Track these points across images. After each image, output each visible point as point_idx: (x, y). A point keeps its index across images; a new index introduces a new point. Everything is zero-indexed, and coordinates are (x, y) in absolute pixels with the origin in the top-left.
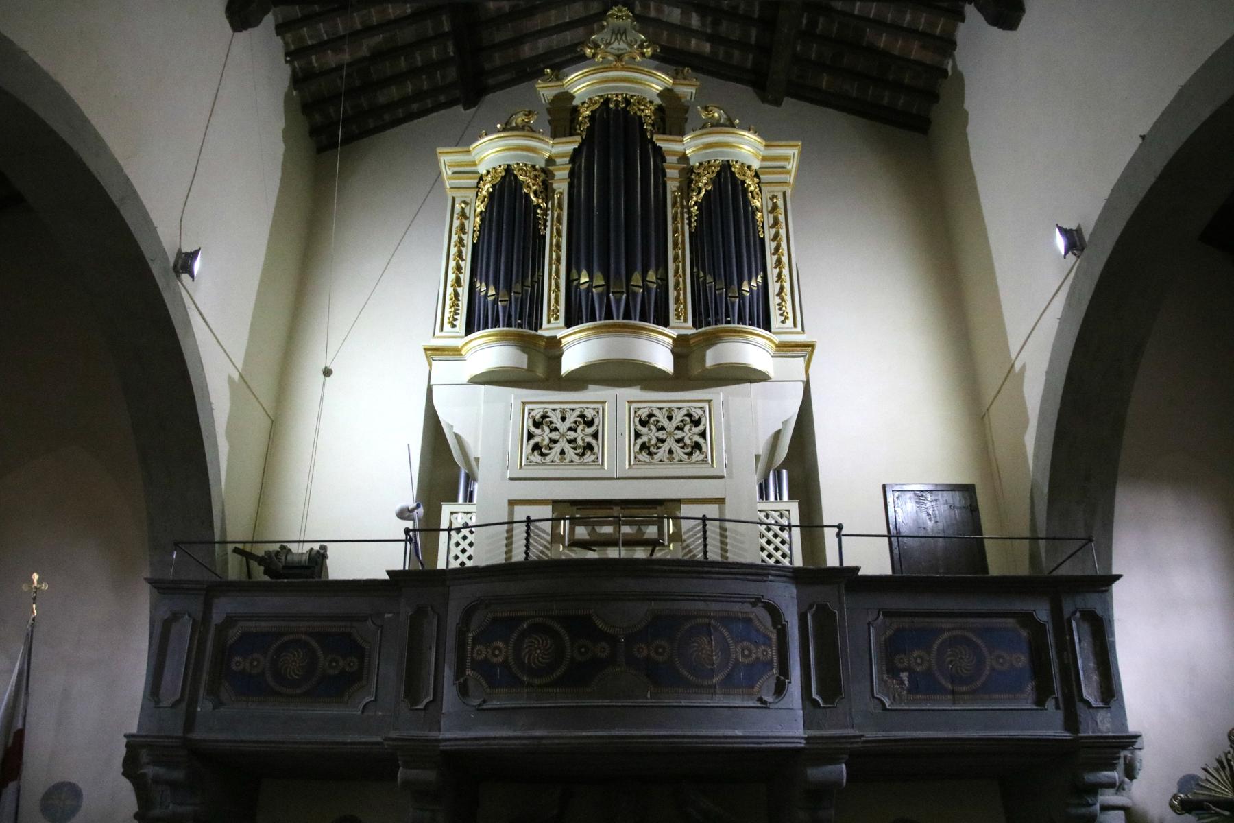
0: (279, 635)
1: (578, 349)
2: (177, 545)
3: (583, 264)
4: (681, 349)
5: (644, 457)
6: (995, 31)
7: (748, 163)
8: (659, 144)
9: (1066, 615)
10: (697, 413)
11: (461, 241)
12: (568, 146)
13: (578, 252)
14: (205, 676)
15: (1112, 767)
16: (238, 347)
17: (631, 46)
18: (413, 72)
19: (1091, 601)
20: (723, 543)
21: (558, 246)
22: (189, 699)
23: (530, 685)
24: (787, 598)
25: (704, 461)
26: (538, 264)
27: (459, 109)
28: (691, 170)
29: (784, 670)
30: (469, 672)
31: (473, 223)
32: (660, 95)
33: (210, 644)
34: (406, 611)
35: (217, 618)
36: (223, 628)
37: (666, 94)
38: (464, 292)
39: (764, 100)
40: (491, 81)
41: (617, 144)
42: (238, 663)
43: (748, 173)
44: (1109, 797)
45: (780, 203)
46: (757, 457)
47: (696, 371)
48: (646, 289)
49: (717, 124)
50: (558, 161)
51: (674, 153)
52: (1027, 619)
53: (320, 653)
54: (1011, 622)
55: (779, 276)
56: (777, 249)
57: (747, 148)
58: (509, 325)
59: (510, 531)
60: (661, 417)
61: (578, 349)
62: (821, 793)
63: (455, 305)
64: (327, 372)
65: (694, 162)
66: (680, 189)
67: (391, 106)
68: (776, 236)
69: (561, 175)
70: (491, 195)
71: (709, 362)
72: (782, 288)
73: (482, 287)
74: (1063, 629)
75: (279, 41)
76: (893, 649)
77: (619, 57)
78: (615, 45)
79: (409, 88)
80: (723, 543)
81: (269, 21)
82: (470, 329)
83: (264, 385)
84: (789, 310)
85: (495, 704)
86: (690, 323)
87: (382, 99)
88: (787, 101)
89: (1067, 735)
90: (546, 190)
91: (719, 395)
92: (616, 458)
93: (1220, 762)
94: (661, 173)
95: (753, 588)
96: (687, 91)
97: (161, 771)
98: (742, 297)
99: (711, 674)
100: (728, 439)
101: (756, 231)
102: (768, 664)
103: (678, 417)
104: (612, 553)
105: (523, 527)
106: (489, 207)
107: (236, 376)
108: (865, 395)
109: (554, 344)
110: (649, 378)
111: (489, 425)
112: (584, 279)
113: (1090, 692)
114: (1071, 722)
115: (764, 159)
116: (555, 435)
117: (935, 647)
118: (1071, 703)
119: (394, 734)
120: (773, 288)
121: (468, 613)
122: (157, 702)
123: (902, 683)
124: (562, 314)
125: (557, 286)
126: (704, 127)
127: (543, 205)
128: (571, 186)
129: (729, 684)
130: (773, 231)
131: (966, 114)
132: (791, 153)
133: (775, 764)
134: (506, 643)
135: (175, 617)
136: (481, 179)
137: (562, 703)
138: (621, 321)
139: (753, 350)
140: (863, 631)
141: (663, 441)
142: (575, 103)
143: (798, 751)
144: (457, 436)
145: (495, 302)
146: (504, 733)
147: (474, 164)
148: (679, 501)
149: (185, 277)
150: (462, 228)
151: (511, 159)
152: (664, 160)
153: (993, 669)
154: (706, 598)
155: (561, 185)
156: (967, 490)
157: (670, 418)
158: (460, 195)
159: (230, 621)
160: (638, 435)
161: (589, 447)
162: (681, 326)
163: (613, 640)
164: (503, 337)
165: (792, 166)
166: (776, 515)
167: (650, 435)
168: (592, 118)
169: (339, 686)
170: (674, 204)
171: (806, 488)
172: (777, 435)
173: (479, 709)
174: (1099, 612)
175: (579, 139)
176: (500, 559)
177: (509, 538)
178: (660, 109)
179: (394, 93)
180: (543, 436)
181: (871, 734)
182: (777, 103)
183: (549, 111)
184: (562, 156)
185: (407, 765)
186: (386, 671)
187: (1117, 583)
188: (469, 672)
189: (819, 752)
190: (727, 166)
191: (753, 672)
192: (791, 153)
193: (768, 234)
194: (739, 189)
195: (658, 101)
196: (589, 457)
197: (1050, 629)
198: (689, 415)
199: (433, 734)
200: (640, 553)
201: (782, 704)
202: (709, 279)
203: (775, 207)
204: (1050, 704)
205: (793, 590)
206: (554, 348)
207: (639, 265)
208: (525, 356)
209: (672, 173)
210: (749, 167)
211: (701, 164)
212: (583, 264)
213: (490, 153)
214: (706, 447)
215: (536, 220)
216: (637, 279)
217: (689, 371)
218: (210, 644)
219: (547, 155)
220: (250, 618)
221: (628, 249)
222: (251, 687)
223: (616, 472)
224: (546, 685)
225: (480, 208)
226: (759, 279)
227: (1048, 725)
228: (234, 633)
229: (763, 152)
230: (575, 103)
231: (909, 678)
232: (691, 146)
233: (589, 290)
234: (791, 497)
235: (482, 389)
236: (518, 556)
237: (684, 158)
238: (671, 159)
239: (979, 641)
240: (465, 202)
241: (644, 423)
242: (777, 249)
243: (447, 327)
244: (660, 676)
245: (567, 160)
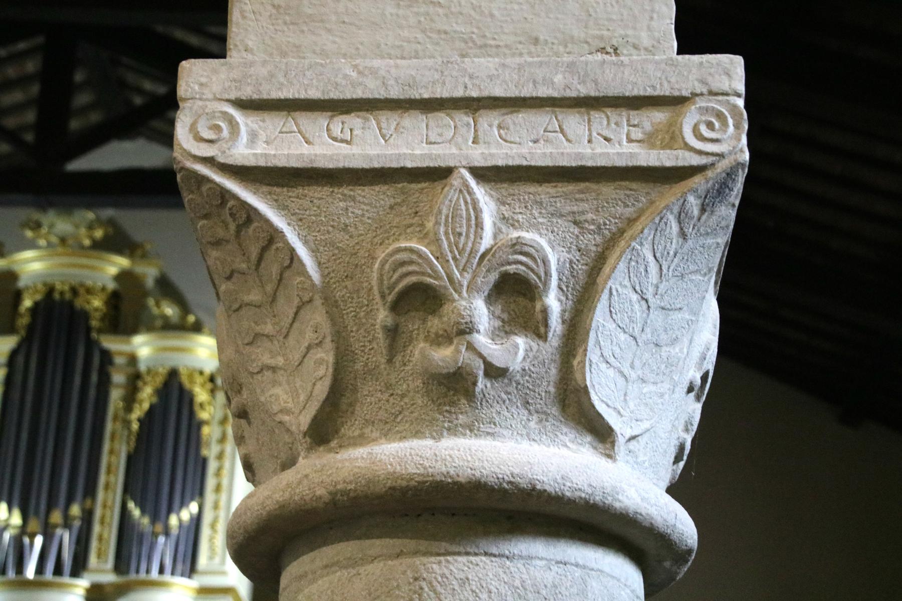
17: (77, 226)
37: (123, 277)
42: (30, 572)
44: (350, 369)
51: (121, 354)
64: (433, 514)
65: (142, 367)
73: (131, 505)
86: (110, 564)
90: (130, 399)
94: (105, 383)
168: (35, 310)
170: (115, 418)
190: (173, 374)
194: (185, 399)
209: (118, 378)
210: (201, 373)
232: (143, 346)
237: (133, 359)
238: (119, 360)
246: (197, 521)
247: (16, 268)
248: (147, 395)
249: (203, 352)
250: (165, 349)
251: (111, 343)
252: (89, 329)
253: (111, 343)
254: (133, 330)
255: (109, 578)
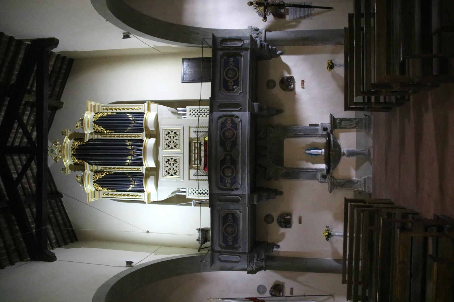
0: (223, 233)
1: (149, 163)
2: (201, 261)
3: (123, 162)
4: (149, 136)
5: (178, 146)
6: (58, 46)
7: (93, 116)
8: (87, 140)
9: (220, 47)
10: (166, 133)
11: (115, 195)
12: (87, 166)
13: (120, 163)
14: (233, 251)
15: (257, 41)
16: (146, 254)
17: (56, 148)
18: (54, 213)
19: (219, 41)
20: (204, 127)
21: (118, 168)
22: (239, 254)
23: (236, 174)
24: (217, 114)
25: (179, 131)
26: (123, 174)
27: (62, 199)
28: (95, 132)
29: (233, 116)
30: (233, 188)
31: (110, 192)
32: (70, 139)
33: (226, 250)
34: (218, 203)
35: (219, 249)
36: (222, 248)
37: (70, 138)
38: (131, 193)
39: (61, 107)
40: (54, 189)
41: (86, 152)
42: (230, 243)
43: (96, 116)
45: (105, 108)
46: (178, 118)
47: (155, 133)
48: (131, 145)
49: (82, 124)
50: (91, 168)
51: (90, 136)
52: (222, 57)
53: (228, 224)
54: (222, 60)
55: (127, 109)
56: (119, 109)
57: (89, 116)
58: (143, 181)
59: (200, 180)
60: (167, 142)
61: (149, 163)
62: (260, 108)
63: (135, 196)
64: (148, 232)
65: (93, 131)
66: (101, 135)
67: (63, 218)
68: (115, 109)
69: (96, 168)
70: (102, 187)
71: (153, 129)
72: (131, 109)
74: (223, 49)
75: (17, 264)
76: (227, 89)
77: (60, 151)
78: (56, 152)
79: (58, 214)
80: (204, 127)
81: (52, 251)
82: (143, 191)
83: (154, 248)
84: (137, 107)
85: (240, 181)
86: (141, 134)
87: (61, 222)
88: (62, 100)
89: (249, 51)
90: (101, 172)
91: (161, 127)
92: (178, 154)
93: (255, 9)
95: (214, 122)
96: (69, 132)
97: (255, 259)
98: (134, 120)
99: (234, 133)
100: (173, 125)
101: (113, 115)
102: (232, 120)
103: (167, 137)
104: (202, 155)
105: (199, 177)
106: (105, 187)
107: (153, 254)
108: (155, 84)
109: (147, 169)
110: (157, 144)
111: (167, 187)
112: (128, 161)
113: (240, 44)
114: (246, 49)
115: (91, 111)
116: (172, 169)
117: (228, 79)
118: (242, 49)
119: (247, 205)
120: (131, 111)
121: (219, 188)
122: (239, 261)
123: (236, 88)
124: (138, 167)
125: (131, 168)
126: (83, 128)
127: (106, 172)
128: (100, 165)
129: (236, 129)
130: (114, 110)
131: (75, 51)
132: (91, 103)
133: (254, 117)
134: (226, 179)
135: (219, 259)
136: (97, 190)
137: (240, 167)
138: (143, 152)
139: (150, 118)
140: (224, 96)
141: (173, 142)
142: (72, 164)
143: (251, 113)
144: (172, 193)
145: (134, 185)
146: (247, 181)
147: (92, 192)
148: (189, 138)
149: (133, 264)
150: (112, 195)
151: (91, 181)
152: (92, 139)
153: (234, 66)
154: (217, 133)
155: (100, 168)
156: (183, 60)
157: (167, 140)
158: (101, 195)
159: (220, 246)
160: (172, 148)
161: (175, 160)
162: (143, 136)
163: (226, 155)
164: (145, 182)
165: (93, 104)
166: (190, 112)
167: (172, 145)
168: (78, 159)
169: (235, 218)
170: (106, 137)
171: (184, 104)
172: (172, 112)
173: (241, 185)
174: (221, 39)
175: (85, 163)
176: (207, 182)
177: (202, 180)
178: (75, 140)
179: (60, 218)
180: (172, 172)
181: (248, 96)
182: (62, 103)
183: (75, 171)
184: (90, 168)
185: (253, 202)
186: (232, 207)
187: (215, 35)
188: (233, 188)
189: (251, 108)
190: (94, 122)
191: (233, 122)
192: (91, 103)
193: (115, 111)
194: (101, 119)
195: (73, 140)
196: (178, 160)
197: (224, 51)
198: (167, 135)
199: (247, 196)
200: (202, 148)
201: (240, 116)
202: (129, 128)
203: (107, 109)
204: (242, 54)
205: (214, 113)
206: (148, 169)
207: (124, 147)
208: (151, 177)
209: (96, 137)
210: (95, 116)
211: (94, 129)
212: (123, 162)
213: (89, 187)
214: (175, 131)
215: (110, 174)
216: (129, 147)
217: (155, 134)
218: (226, 250)
219: (90, 172)
220: (219, 242)
221: (116, 151)
222: (236, 240)
223: (181, 153)
224: (236, 170)
225: (106, 190)
226: (128, 115)
227: (247, 54)
228: (223, 245)
229: (89, 112)
230: (72, 164)
231: (235, 86)
232: (88, 131)
233: (131, 160)
234: (185, 107)
235: (158, 188)
236: (206, 178)
237: (91, 134)
238: (91, 137)
239: (227, 68)
240: (104, 194)
241: (169, 146)
242: (119, 109)
243: (141, 197)
244: (234, 144)
245: (91, 166)
246: (131, 113)
247: (68, 165)
248: (99, 128)
249: (89, 116)
250: (88, 126)
251: (87, 139)
252: (83, 145)
253: (87, 139)
254: (84, 134)
255: (144, 133)
